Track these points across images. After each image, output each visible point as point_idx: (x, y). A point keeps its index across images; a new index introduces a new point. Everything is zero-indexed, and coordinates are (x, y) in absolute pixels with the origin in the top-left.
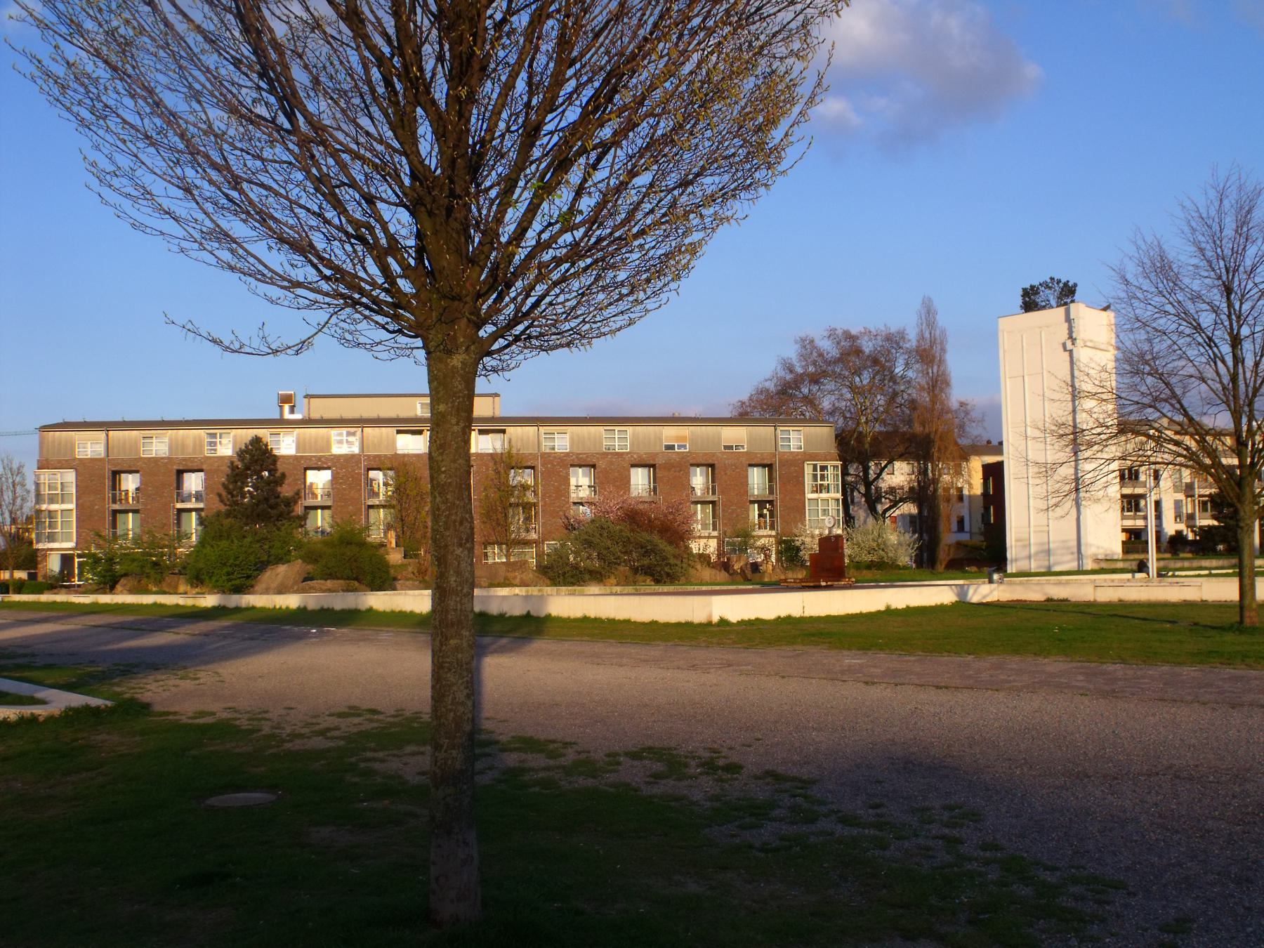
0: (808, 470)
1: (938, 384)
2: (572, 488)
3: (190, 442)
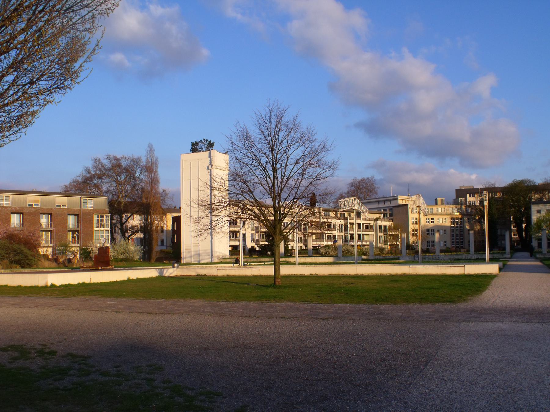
0: (95, 217)
1: (154, 181)
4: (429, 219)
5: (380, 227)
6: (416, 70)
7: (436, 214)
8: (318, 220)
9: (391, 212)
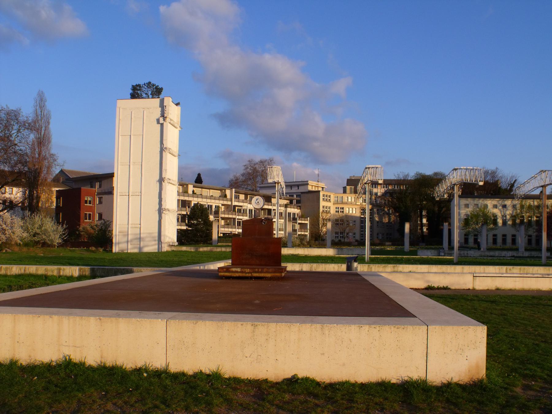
1: (42, 142)
4: (338, 208)
5: (290, 214)
6: (281, 66)
7: (346, 203)
8: (229, 203)
9: (298, 199)
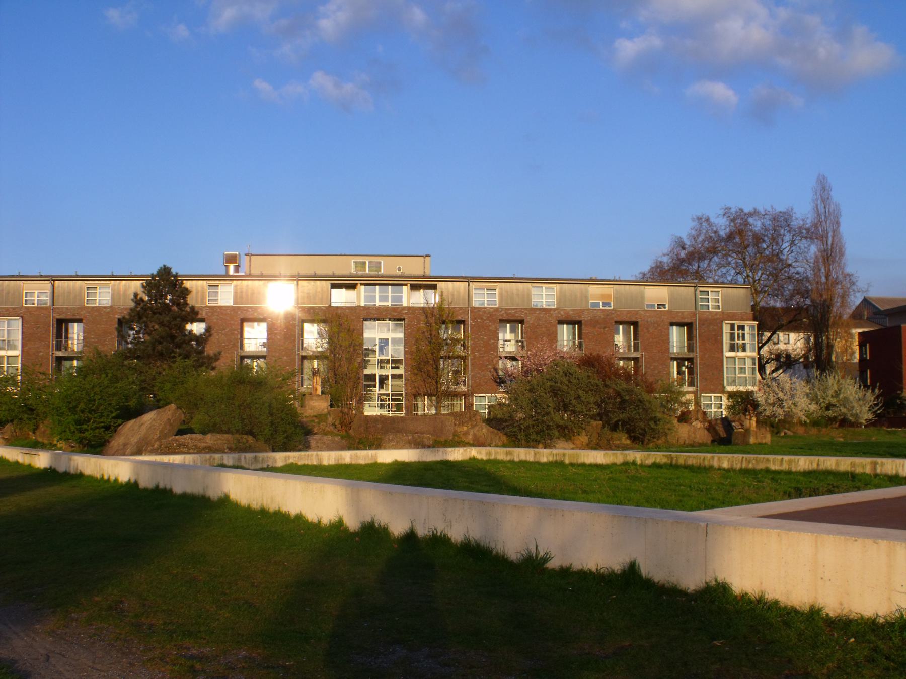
0: (726, 329)
1: (830, 256)
2: (501, 342)
3: (122, 289)
